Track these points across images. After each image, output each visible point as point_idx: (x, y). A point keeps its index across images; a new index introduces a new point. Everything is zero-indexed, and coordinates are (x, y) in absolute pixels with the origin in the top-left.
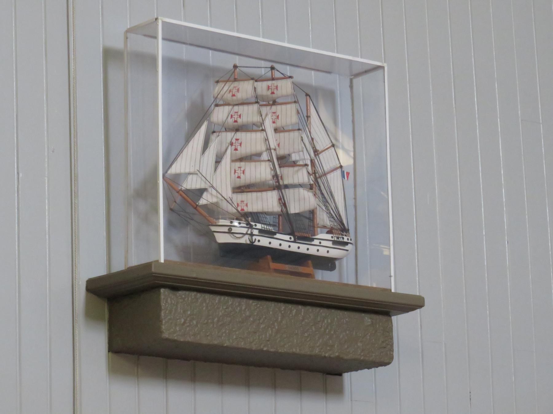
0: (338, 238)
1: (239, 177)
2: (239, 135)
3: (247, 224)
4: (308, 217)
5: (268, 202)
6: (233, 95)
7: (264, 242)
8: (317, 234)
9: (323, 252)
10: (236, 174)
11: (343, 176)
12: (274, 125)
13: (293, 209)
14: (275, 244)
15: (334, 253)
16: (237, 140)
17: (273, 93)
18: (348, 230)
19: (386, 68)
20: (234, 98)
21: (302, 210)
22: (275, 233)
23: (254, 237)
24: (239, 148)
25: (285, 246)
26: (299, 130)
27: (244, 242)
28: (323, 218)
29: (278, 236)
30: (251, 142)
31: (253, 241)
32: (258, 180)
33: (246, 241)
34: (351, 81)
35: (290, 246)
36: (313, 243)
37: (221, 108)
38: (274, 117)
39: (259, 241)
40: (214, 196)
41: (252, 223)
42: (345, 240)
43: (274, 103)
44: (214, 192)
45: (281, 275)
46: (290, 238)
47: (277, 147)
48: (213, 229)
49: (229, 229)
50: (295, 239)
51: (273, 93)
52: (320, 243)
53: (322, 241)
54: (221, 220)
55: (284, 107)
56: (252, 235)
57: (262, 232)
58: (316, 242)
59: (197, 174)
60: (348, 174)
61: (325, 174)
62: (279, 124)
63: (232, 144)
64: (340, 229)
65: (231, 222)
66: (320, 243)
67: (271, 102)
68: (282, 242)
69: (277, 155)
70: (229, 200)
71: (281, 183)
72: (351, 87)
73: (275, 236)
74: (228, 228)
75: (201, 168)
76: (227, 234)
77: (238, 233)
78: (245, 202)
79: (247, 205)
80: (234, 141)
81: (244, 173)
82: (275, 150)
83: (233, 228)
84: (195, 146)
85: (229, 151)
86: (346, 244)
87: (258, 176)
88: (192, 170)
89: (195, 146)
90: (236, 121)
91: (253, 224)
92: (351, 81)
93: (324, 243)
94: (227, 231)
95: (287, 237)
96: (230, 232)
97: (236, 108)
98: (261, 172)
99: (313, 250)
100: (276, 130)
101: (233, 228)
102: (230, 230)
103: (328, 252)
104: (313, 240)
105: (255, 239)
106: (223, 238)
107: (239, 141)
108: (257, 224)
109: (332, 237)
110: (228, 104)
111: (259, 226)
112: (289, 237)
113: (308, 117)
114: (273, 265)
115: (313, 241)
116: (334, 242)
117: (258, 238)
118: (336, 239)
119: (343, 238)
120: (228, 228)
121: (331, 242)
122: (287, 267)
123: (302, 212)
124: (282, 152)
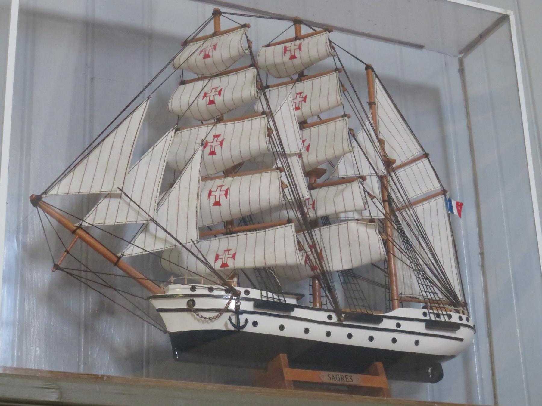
0: (438, 315)
1: (217, 203)
2: (220, 128)
3: (227, 291)
4: (384, 283)
5: (279, 247)
6: (207, 56)
7: (268, 325)
8: (393, 309)
9: (405, 344)
10: (212, 198)
11: (450, 208)
12: (298, 113)
13: (338, 261)
14: (293, 329)
15: (432, 345)
16: (216, 136)
17: (293, 57)
18: (465, 305)
19: (512, 18)
20: (208, 60)
21: (356, 263)
22: (291, 308)
23: (243, 318)
24: (218, 150)
25: (317, 334)
26: (344, 116)
27: (224, 328)
28: (406, 280)
29: (298, 312)
30: (244, 137)
31: (242, 323)
32: (255, 207)
33: (226, 325)
34: (461, 63)
35: (328, 334)
36: (381, 326)
37: (189, 86)
38: (299, 99)
39: (255, 324)
40: (161, 239)
41: (237, 288)
42: (455, 318)
43: (302, 77)
44: (161, 233)
45: (308, 392)
46: (330, 317)
47: (303, 151)
48: (158, 304)
49: (188, 304)
50: (339, 320)
51: (293, 57)
52: (398, 325)
53: (400, 322)
54: (171, 286)
55: (317, 81)
56: (238, 312)
57: (261, 306)
58: (386, 324)
59: (120, 196)
60: (460, 205)
61: (411, 205)
62: (306, 109)
63: (204, 144)
64: (445, 306)
65: (193, 289)
66: (398, 325)
67: (296, 77)
68: (309, 324)
69: (303, 166)
70: (189, 246)
71: (311, 214)
72: (462, 71)
73: (293, 314)
74: (186, 300)
75: (151, 196)
76: (185, 314)
77: (217, 310)
78: (232, 252)
79: (234, 256)
80: (210, 138)
81: (226, 195)
82: (300, 155)
83: (196, 300)
84: (118, 145)
85: (198, 157)
86: (456, 327)
87: (254, 197)
88: (106, 189)
89: (118, 145)
90: (212, 102)
91: (242, 290)
92: (461, 63)
93: (405, 326)
94: (185, 306)
95: (322, 316)
96: (191, 308)
97: (216, 82)
98: (260, 190)
99: (382, 341)
100: (303, 124)
101: (196, 300)
102: (191, 303)
103: (417, 343)
104: (379, 319)
105: (247, 321)
106: (180, 323)
107: (220, 139)
108: (251, 290)
109: (425, 314)
110: (203, 78)
111: (255, 294)
112: (327, 314)
113: (372, 104)
114: (291, 374)
115: (382, 321)
116: (430, 324)
117: (252, 318)
118: (433, 318)
119: (450, 316)
120: (186, 300)
121: (423, 324)
122: (324, 376)
123: (357, 268)
124: (311, 158)
